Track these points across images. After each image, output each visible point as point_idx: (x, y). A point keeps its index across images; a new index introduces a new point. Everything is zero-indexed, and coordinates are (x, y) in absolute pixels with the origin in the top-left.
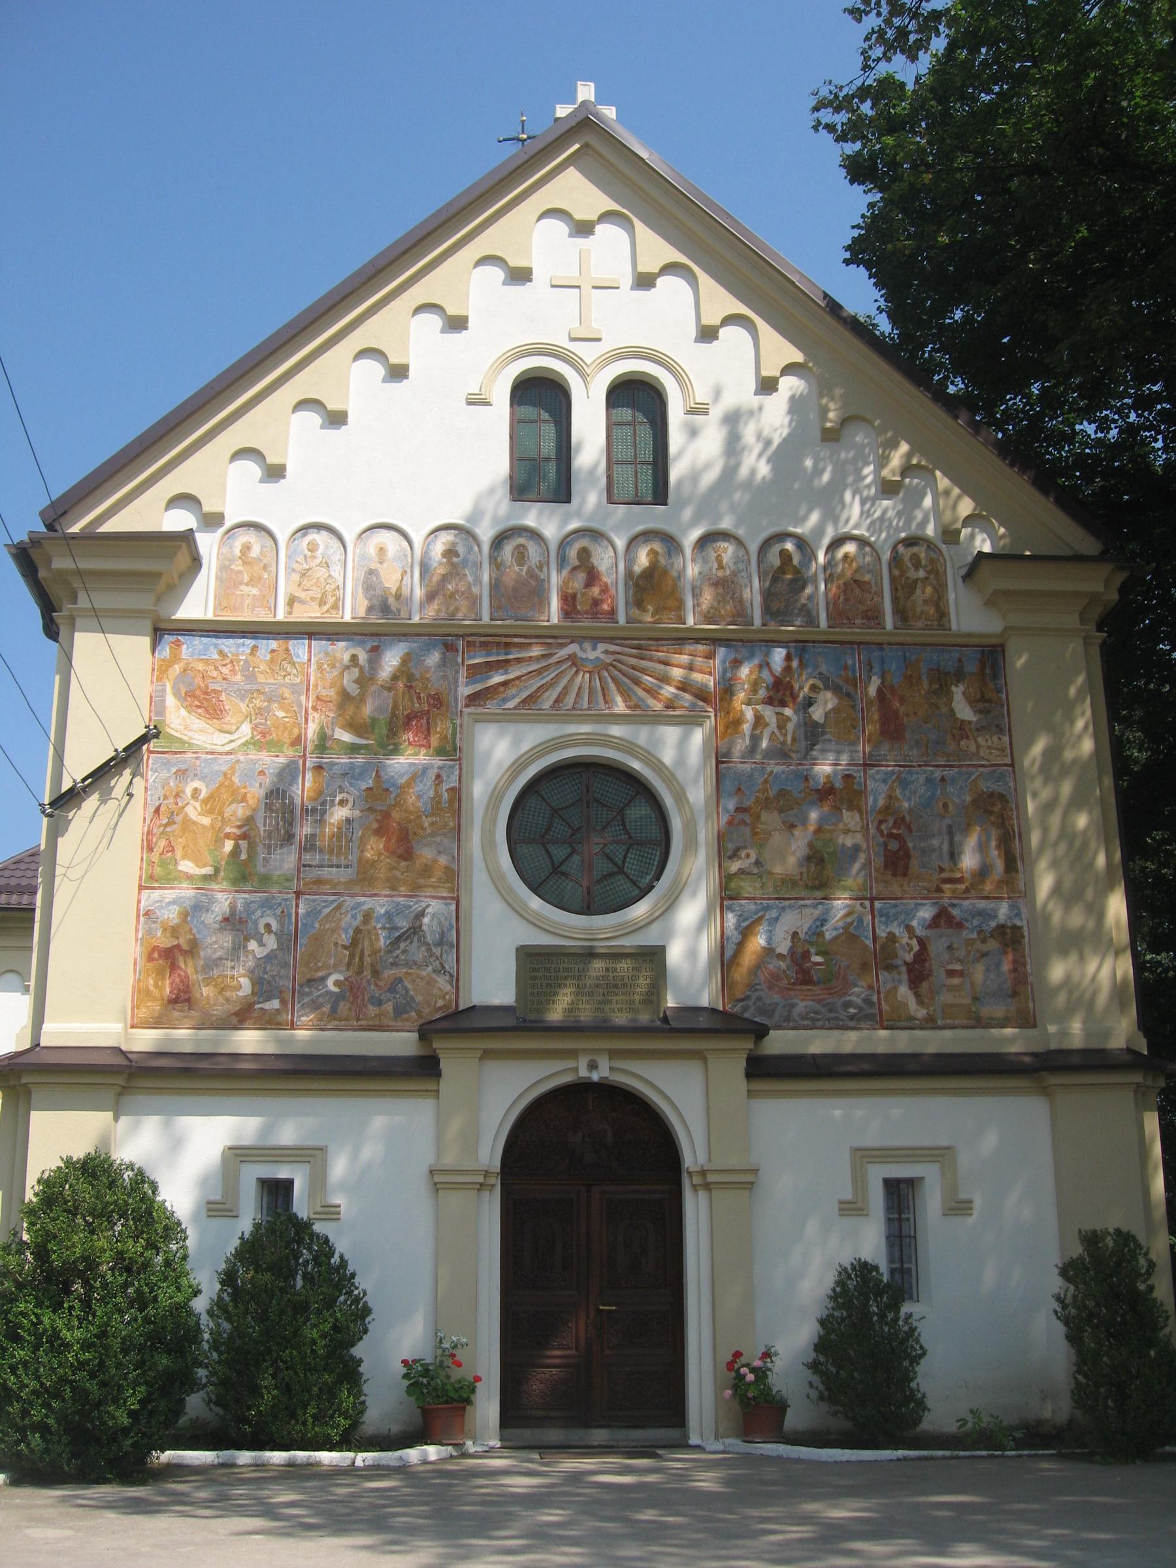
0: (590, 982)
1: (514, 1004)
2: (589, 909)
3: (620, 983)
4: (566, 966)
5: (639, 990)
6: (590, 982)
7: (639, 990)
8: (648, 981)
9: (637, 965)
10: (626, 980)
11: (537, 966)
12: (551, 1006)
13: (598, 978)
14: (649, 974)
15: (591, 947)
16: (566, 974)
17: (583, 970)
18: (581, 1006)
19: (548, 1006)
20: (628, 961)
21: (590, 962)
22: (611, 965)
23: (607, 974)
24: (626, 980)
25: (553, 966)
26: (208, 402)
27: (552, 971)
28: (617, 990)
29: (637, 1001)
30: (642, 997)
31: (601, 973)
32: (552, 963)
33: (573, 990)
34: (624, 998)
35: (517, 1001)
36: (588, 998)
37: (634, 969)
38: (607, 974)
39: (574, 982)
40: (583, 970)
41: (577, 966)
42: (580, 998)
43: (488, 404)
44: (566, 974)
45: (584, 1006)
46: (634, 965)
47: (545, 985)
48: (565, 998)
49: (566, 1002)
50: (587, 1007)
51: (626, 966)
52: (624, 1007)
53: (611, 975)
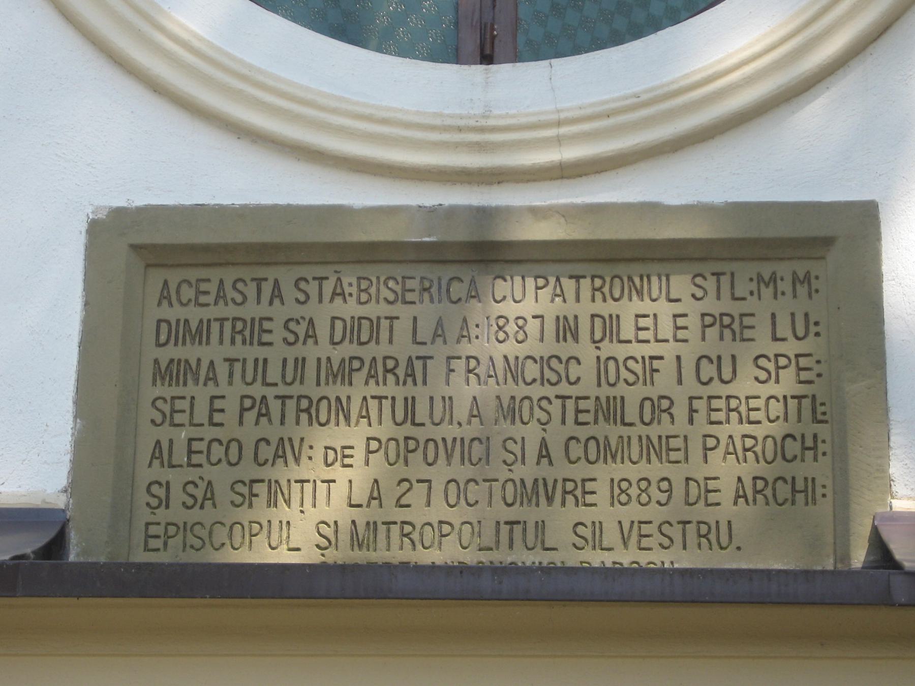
0: (474, 388)
1: (61, 502)
2: (516, 56)
3: (633, 395)
4: (350, 309)
5: (737, 429)
6: (474, 388)
7: (737, 429)
8: (787, 383)
9: (726, 305)
10: (664, 383)
11: (195, 315)
12: (261, 511)
13: (514, 369)
14: (791, 347)
15: (484, 214)
16: (348, 349)
17: (439, 333)
18: (417, 514)
19: (244, 515)
20: (681, 284)
21: (474, 295)
22: (585, 308)
23: (566, 349)
24: (664, 383)
25: (279, 312)
26: (743, 602)
27: (278, 335)
28: (614, 432)
29: (727, 489)
30: (749, 469)
31: (532, 347)
32: (277, 294)
33: (385, 430)
34: (655, 469)
35: (74, 486)
36: (462, 472)
37: (708, 321)
38: (566, 349)
39: (390, 389)
40: (439, 333)
41: (405, 313)
42: (417, 468)
43: (149, 467)
44: (348, 349)
45: (439, 511)
46: (711, 305)
47: (231, 406)
48: (338, 472)
49: (340, 491)
50: (455, 516)
51: (665, 310)
52: (654, 513)
53: (586, 350)
